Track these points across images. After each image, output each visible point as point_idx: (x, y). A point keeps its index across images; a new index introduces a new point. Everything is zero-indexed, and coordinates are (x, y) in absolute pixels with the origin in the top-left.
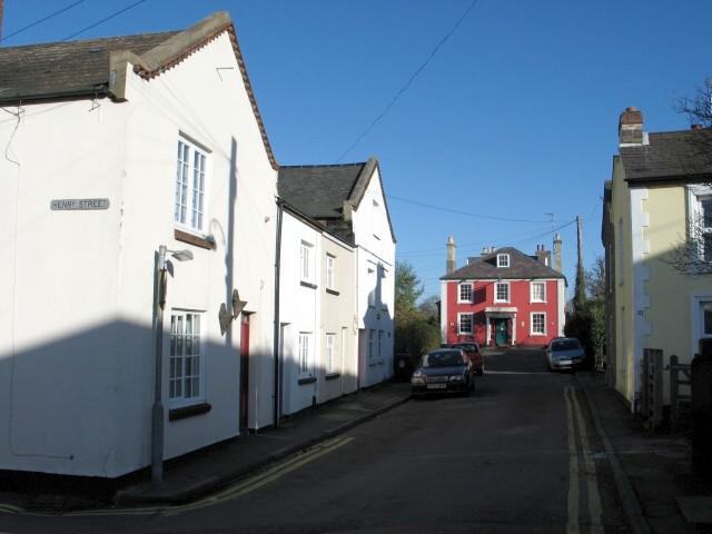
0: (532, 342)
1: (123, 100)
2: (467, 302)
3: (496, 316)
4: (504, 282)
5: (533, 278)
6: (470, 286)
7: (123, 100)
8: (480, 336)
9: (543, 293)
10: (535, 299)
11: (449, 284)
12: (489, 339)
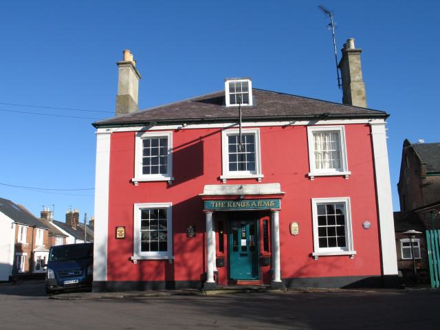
0: (323, 272)
1: (389, 115)
2: (159, 177)
3: (233, 206)
4: (248, 128)
5: (314, 119)
6: (164, 141)
7: (389, 115)
8: (193, 259)
9: (337, 155)
10: (320, 167)
11: (114, 136)
12: (212, 268)
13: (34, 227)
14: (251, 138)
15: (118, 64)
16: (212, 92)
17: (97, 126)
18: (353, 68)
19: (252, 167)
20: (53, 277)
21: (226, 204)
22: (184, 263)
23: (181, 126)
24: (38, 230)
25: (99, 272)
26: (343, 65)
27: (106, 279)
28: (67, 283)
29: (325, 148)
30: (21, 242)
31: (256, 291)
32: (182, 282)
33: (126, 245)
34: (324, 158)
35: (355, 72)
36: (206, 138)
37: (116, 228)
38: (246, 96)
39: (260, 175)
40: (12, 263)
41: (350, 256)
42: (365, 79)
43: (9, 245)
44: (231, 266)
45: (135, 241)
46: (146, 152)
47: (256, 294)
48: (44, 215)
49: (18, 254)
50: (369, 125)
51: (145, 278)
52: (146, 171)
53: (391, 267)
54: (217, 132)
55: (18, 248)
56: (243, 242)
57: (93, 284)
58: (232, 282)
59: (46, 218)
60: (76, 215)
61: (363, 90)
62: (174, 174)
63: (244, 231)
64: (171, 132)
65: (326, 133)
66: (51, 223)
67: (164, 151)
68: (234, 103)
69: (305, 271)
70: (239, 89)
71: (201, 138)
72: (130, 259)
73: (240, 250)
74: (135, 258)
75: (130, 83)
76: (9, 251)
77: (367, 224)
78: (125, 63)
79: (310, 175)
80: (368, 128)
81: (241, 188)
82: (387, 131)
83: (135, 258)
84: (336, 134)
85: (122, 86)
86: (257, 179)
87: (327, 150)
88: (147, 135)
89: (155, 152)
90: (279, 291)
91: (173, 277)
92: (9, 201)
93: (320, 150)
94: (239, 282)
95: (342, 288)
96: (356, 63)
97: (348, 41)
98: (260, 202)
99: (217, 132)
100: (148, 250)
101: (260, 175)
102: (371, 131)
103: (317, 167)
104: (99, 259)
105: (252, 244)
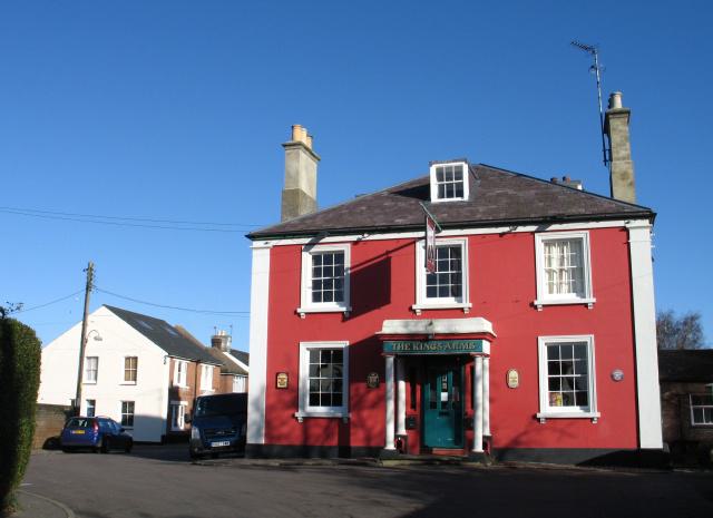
0: (551, 441)
2: (333, 306)
3: (418, 349)
4: (451, 238)
5: (544, 222)
6: (340, 256)
9: (578, 273)
10: (552, 290)
11: (275, 251)
13: (198, 362)
14: (456, 251)
15: (285, 146)
16: (405, 179)
17: (253, 237)
18: (616, 138)
19: (457, 293)
20: (198, 437)
21: (411, 347)
22: (362, 424)
23: (360, 236)
24: (204, 366)
25: (255, 434)
26: (606, 130)
27: (263, 441)
28: (214, 445)
29: (562, 264)
30: (180, 385)
31: (447, 463)
32: (359, 448)
33: (287, 397)
34: (561, 277)
35: (621, 145)
36: (396, 253)
37: (277, 374)
38: (460, 186)
39: (466, 304)
40: (164, 415)
41: (592, 419)
42: (635, 156)
43: (160, 390)
44: (427, 428)
45: (300, 393)
46: (316, 272)
47: (446, 467)
48: (216, 342)
49: (173, 402)
50: (625, 230)
51: (311, 442)
52: (316, 298)
53: (652, 436)
54: (411, 244)
55: (174, 394)
56: (444, 396)
57: (246, 447)
58: (426, 449)
59: (219, 348)
60: (132, 404)
61: (631, 171)
62: (353, 303)
63: (445, 380)
64: (349, 245)
65: (562, 243)
66: (227, 354)
67: (340, 270)
68: (452, 196)
69: (524, 439)
70: (449, 178)
71: (388, 252)
72: (293, 416)
73: (439, 406)
74: (300, 415)
75: (305, 174)
76: (161, 398)
77: (618, 374)
78: (294, 145)
79: (536, 303)
80: (625, 233)
81: (431, 324)
82: (652, 238)
83: (300, 415)
84: (577, 243)
85: (291, 177)
86: (462, 309)
87: (566, 267)
88: (317, 249)
89: (328, 272)
90: (478, 464)
91: (349, 441)
92: (162, 322)
93: (555, 265)
94: (435, 451)
95: (578, 465)
96: (621, 131)
97: (612, 95)
98: (455, 343)
99: (411, 244)
100: (318, 405)
101: (466, 304)
102: (628, 238)
103: (551, 291)
104: (254, 416)
105: (456, 398)
